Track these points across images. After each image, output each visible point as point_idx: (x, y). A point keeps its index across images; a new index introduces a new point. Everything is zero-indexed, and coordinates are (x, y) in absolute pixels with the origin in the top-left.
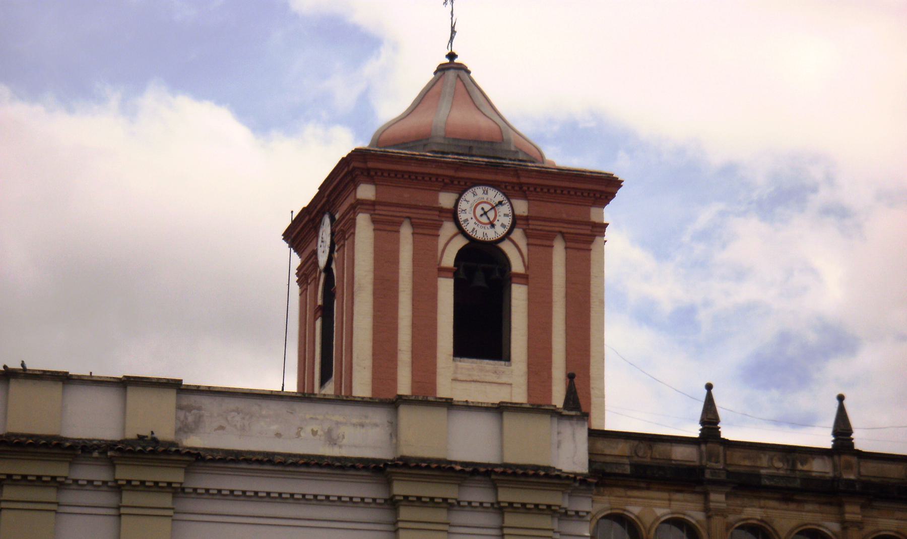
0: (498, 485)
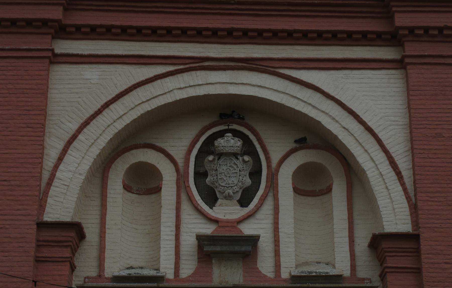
0: (394, 9)
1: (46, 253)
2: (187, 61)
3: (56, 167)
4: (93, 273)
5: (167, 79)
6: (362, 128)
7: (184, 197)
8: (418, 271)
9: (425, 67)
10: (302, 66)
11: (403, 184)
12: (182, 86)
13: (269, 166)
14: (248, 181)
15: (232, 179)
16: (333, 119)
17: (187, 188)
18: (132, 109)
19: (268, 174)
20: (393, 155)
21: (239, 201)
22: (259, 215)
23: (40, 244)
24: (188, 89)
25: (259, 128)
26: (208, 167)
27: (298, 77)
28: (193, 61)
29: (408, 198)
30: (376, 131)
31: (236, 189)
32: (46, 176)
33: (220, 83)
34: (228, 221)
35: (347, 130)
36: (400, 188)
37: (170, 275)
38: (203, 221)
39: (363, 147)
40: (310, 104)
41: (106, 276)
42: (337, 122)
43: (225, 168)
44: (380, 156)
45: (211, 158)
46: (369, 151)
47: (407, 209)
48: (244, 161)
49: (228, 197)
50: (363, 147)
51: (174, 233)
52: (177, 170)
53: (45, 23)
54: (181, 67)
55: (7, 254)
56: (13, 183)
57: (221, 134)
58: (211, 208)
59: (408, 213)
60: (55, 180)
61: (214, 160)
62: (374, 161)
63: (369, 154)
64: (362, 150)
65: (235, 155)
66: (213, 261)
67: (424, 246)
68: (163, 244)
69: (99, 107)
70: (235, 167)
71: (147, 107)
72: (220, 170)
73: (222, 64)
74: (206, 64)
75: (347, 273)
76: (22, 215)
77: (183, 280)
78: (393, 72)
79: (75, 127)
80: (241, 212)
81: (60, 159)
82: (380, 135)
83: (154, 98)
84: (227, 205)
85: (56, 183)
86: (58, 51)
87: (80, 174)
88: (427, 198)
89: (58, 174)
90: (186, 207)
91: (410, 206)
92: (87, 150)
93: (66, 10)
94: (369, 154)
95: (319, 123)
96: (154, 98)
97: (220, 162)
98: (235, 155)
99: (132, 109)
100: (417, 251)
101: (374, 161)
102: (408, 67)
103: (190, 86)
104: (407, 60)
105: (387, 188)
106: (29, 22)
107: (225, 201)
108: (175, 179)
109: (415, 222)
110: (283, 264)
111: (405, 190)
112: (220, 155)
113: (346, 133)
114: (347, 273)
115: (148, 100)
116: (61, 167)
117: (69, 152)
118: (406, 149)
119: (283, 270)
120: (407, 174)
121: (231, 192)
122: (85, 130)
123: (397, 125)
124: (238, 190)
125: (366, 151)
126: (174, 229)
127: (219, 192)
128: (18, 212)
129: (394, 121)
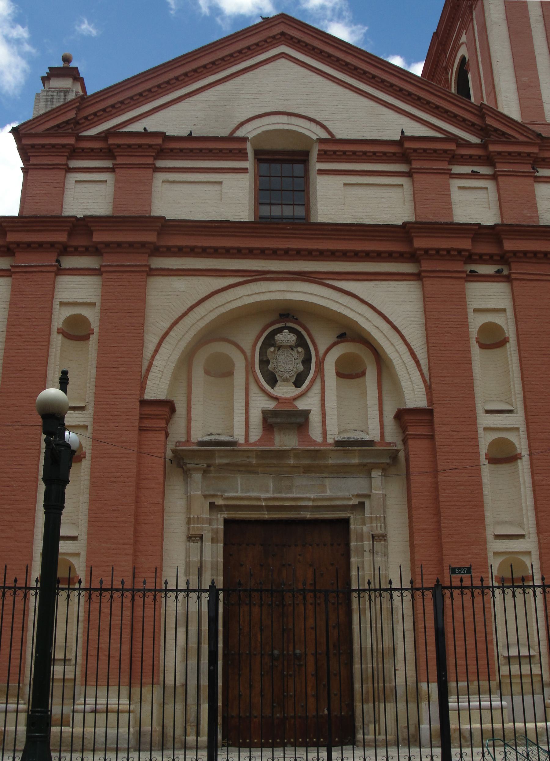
1: (147, 424)
2: (253, 274)
3: (153, 357)
4: (183, 439)
5: (238, 288)
6: (390, 326)
7: (251, 380)
8: (432, 437)
9: (438, 279)
10: (343, 278)
11: (420, 370)
12: (250, 293)
13: (317, 356)
14: (301, 368)
15: (289, 366)
16: (367, 319)
17: (254, 372)
18: (211, 311)
19: (316, 362)
20: (413, 347)
21: (294, 383)
22: (310, 394)
23: (142, 417)
24: (254, 296)
25: (309, 326)
26: (269, 356)
27: (339, 286)
28: (257, 274)
29: (424, 381)
30: (400, 329)
31: (292, 373)
32: (146, 364)
33: (279, 291)
34: (286, 399)
35: (377, 328)
36: (418, 373)
37: (242, 441)
38: (266, 398)
39: (390, 341)
40: (349, 308)
41: (193, 441)
42: (370, 321)
43: (283, 357)
44: (403, 349)
45: (272, 349)
46: (395, 345)
47: (424, 390)
48: (298, 352)
49: (286, 380)
50: (390, 341)
51: (244, 408)
52: (246, 359)
53: (143, 245)
54: (249, 278)
55: (117, 425)
56: (121, 369)
57: (279, 331)
58: (273, 388)
59: (425, 393)
60: (152, 367)
61: (275, 350)
62: (398, 353)
63: (394, 347)
64: (390, 344)
65: (291, 348)
66: (275, 430)
67: (437, 418)
68: (236, 416)
69: (185, 309)
70: (291, 356)
71: (223, 310)
72: (279, 359)
73: (281, 276)
74: (268, 276)
75: (377, 438)
76: (129, 394)
77: (252, 445)
78: (412, 282)
79: (167, 325)
80: (296, 391)
81: (156, 351)
82: (403, 332)
83: (228, 303)
84: (284, 386)
85: (153, 369)
86: (153, 266)
87: (172, 362)
88: (439, 381)
89: (155, 363)
90: (253, 388)
91: (426, 387)
92: (177, 344)
93: (159, 234)
94: (394, 347)
95: (356, 322)
96: (228, 303)
97: (280, 352)
98: (291, 348)
99: (211, 311)
100: (431, 423)
101: (398, 353)
102: (424, 279)
103: (256, 294)
104: (423, 274)
105: (408, 373)
106: (131, 245)
107: (283, 383)
108: (244, 365)
109: (430, 401)
110: (328, 432)
111: (422, 375)
112: (279, 348)
113: (377, 330)
114: (377, 438)
115: (223, 305)
116: (157, 357)
117: (163, 345)
118: (423, 343)
119: (328, 437)
120: (424, 363)
121: (288, 376)
122: (175, 328)
123: (416, 324)
124: (293, 374)
125: (392, 344)
126: (244, 404)
127: (279, 375)
128: (125, 392)
129: (413, 321)
